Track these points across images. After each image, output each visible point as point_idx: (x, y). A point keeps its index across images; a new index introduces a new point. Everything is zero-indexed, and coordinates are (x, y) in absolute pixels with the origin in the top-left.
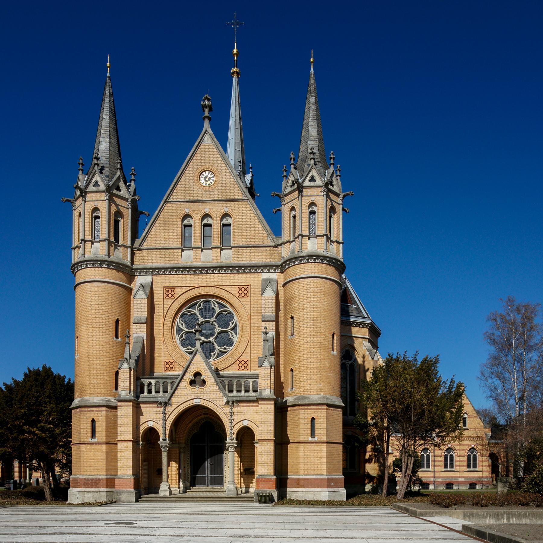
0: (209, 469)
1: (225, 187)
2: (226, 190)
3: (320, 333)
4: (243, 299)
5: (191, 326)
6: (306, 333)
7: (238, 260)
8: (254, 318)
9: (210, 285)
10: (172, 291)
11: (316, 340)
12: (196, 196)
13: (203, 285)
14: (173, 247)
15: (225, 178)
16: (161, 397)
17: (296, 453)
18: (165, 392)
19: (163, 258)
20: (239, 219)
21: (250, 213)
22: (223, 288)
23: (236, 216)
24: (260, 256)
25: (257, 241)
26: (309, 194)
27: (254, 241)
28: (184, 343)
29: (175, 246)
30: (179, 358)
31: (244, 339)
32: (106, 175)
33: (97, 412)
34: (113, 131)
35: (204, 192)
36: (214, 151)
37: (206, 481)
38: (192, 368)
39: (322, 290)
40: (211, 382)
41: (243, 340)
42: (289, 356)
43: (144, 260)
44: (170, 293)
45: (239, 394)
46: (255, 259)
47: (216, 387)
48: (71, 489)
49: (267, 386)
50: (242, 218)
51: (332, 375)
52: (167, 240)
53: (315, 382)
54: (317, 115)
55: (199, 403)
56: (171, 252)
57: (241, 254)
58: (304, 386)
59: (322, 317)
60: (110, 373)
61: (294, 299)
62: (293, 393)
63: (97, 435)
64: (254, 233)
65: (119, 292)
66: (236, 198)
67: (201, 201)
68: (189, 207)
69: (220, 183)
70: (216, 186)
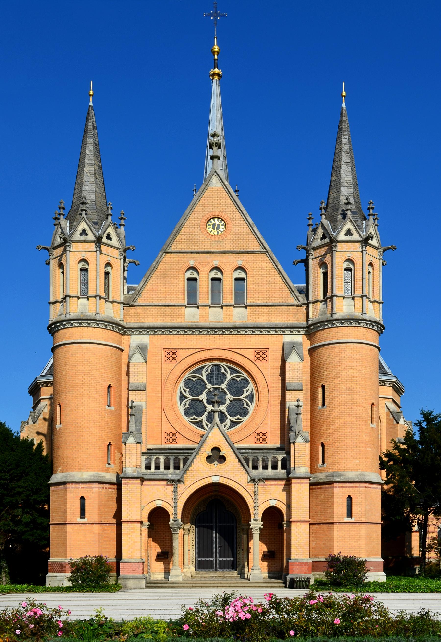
0: (218, 552)
1: (238, 237)
2: (240, 240)
3: (357, 405)
4: (261, 363)
5: (196, 392)
6: (340, 404)
7: (254, 320)
8: (274, 385)
9: (221, 347)
10: (174, 353)
11: (352, 412)
12: (202, 246)
13: (212, 347)
14: (174, 304)
15: (238, 227)
16: (171, 473)
17: (328, 535)
18: (177, 467)
19: (163, 316)
20: (256, 274)
21: (269, 267)
22: (237, 352)
23: (252, 270)
24: (282, 316)
25: (278, 298)
26: (344, 250)
27: (274, 298)
28: (188, 412)
29: (177, 302)
30: (183, 429)
31: (263, 408)
32: (95, 222)
33: (87, 489)
34: (98, 169)
35: (212, 242)
36: (225, 195)
37: (214, 565)
38: (209, 443)
39: (360, 357)
40: (232, 458)
41: (261, 410)
42: (319, 429)
43: (138, 318)
44: (171, 356)
45: (265, 471)
46: (275, 320)
47: (238, 464)
48: (49, 574)
49: (301, 463)
50: (259, 272)
51: (370, 449)
52: (166, 295)
53: (352, 458)
54: (351, 157)
55: (218, 481)
56: (172, 309)
57: (258, 313)
58: (338, 462)
59: (360, 386)
60: (102, 446)
61: (326, 366)
62: (324, 470)
63: (87, 514)
64: (274, 290)
65: (111, 354)
66: (252, 250)
67: (209, 252)
68: (194, 258)
69: (232, 232)
70: (227, 235)
